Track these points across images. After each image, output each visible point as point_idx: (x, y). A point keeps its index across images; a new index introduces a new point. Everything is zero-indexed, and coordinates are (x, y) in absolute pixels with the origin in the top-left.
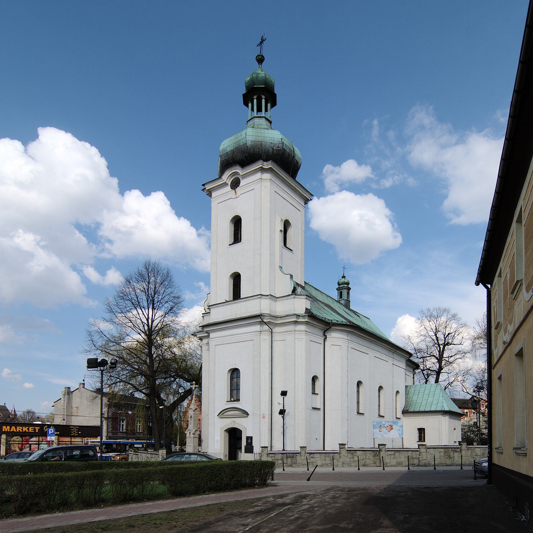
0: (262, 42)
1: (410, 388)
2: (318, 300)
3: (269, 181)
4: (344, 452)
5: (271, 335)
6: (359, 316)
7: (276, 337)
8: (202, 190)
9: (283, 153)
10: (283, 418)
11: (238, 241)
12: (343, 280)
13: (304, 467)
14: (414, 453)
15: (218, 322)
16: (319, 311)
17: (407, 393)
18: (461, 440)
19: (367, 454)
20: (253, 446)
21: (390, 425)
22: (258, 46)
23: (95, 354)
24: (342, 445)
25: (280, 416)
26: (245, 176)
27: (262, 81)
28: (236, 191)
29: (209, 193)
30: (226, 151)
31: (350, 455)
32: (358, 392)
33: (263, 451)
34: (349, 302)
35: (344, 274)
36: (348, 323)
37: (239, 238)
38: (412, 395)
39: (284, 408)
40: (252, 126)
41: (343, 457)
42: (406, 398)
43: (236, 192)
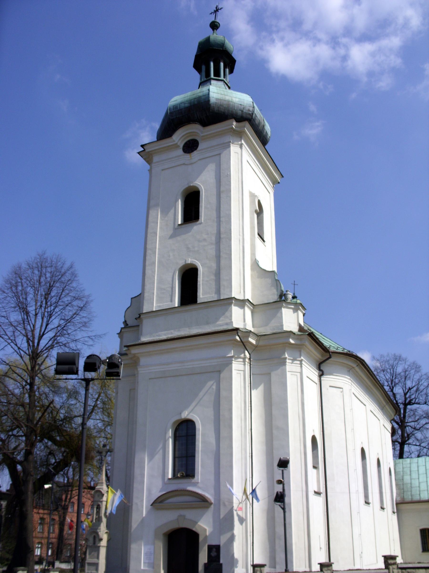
8: (138, 153)
18: (123, 326)
22: (211, 14)
23: (33, 273)
25: (321, 547)
26: (206, 138)
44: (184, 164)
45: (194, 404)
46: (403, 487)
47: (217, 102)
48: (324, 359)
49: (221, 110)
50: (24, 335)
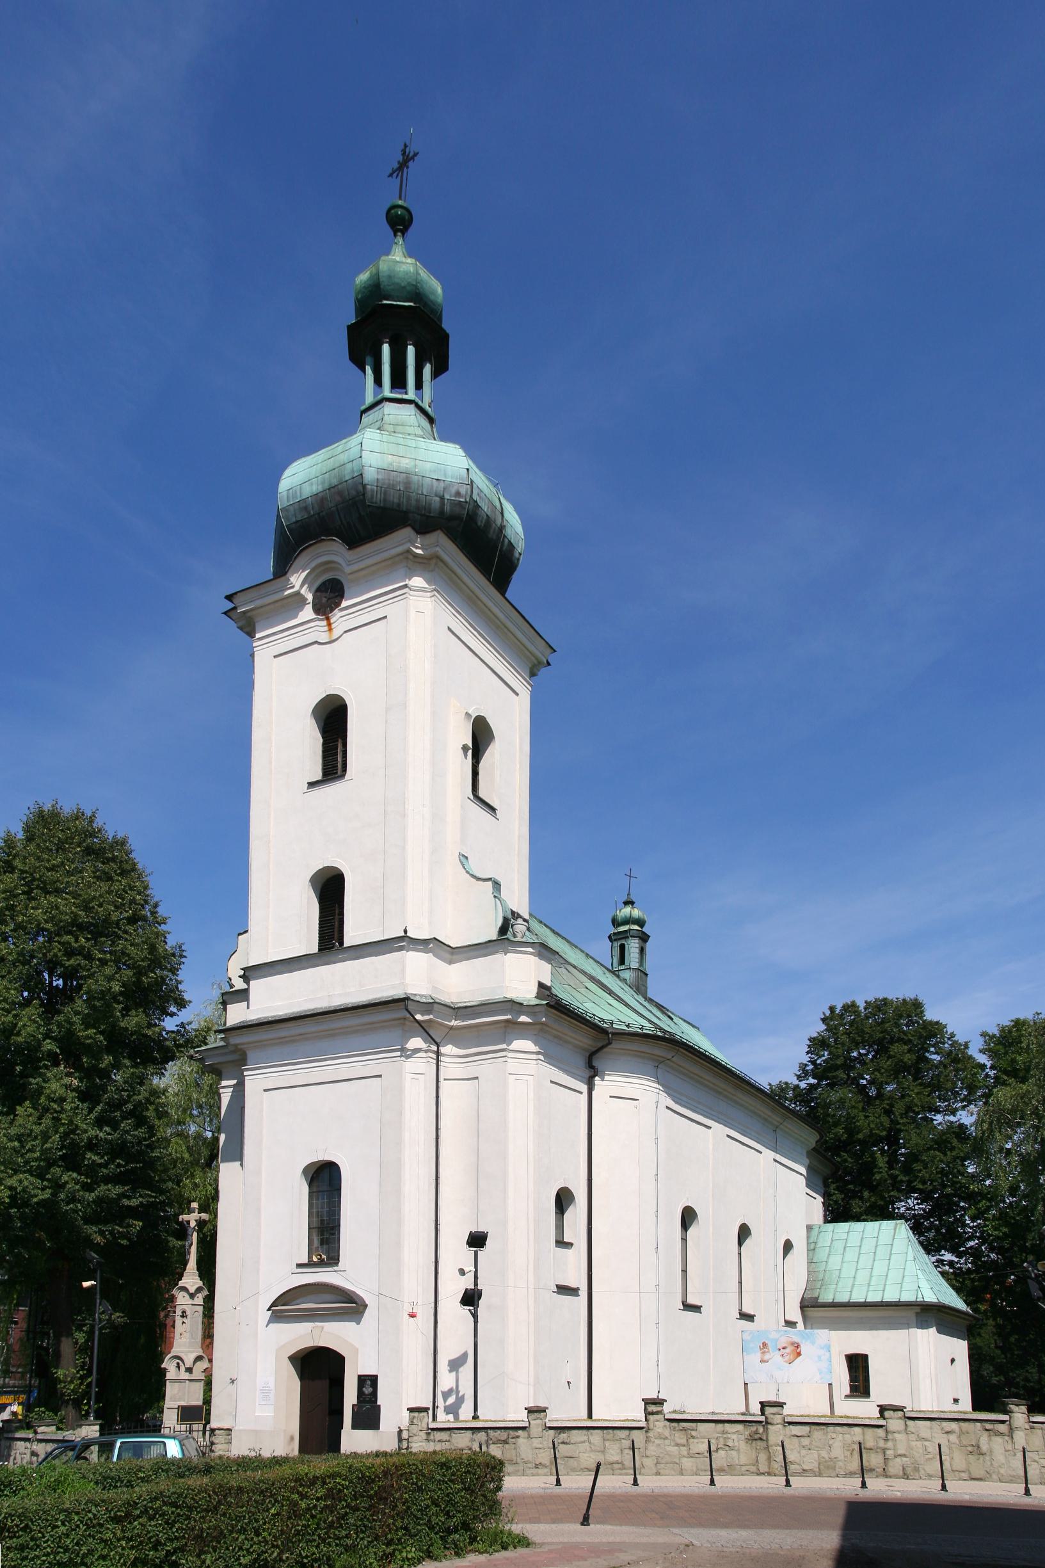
0: (403, 165)
1: (820, 1232)
2: (569, 964)
3: (432, 594)
4: (659, 1426)
5: (435, 1061)
6: (672, 1019)
7: (450, 1068)
8: (225, 613)
9: (470, 513)
10: (475, 1316)
11: (337, 773)
12: (627, 911)
13: (538, 1475)
14: (869, 1431)
15: (272, 1017)
16: (575, 994)
17: (812, 1249)
19: (727, 1433)
20: (379, 1406)
21: (792, 1344)
22: (391, 175)
24: (653, 1404)
25: (465, 1311)
27: (408, 288)
28: (332, 621)
29: (249, 627)
30: (298, 494)
31: (680, 1438)
32: (684, 1240)
33: (415, 1421)
34: (644, 976)
35: (629, 894)
36: (659, 1033)
37: (340, 766)
38: (827, 1252)
39: (476, 1284)
40: (378, 424)
41: (657, 1441)
42: (810, 1262)
43: (329, 624)
46: (824, 1276)
47: (380, 477)
48: (600, 1045)
49: (392, 498)
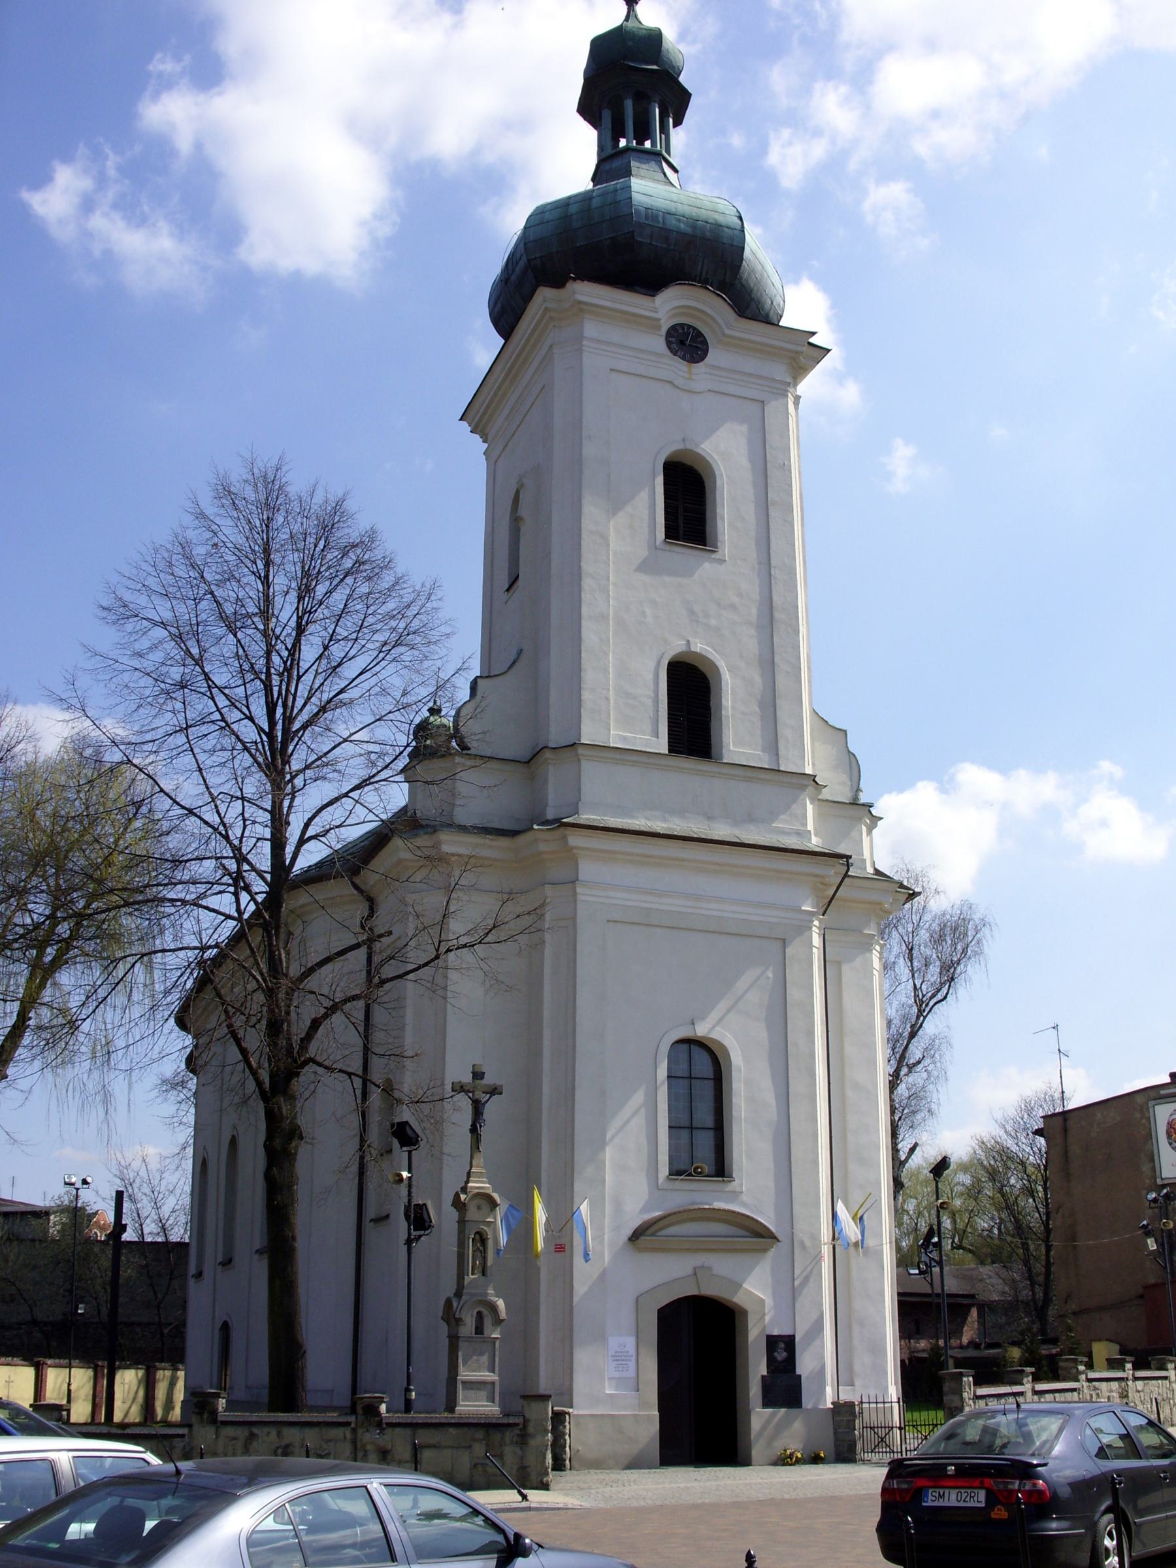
44: (671, 383)
45: (723, 1006)
50: (209, 697)
